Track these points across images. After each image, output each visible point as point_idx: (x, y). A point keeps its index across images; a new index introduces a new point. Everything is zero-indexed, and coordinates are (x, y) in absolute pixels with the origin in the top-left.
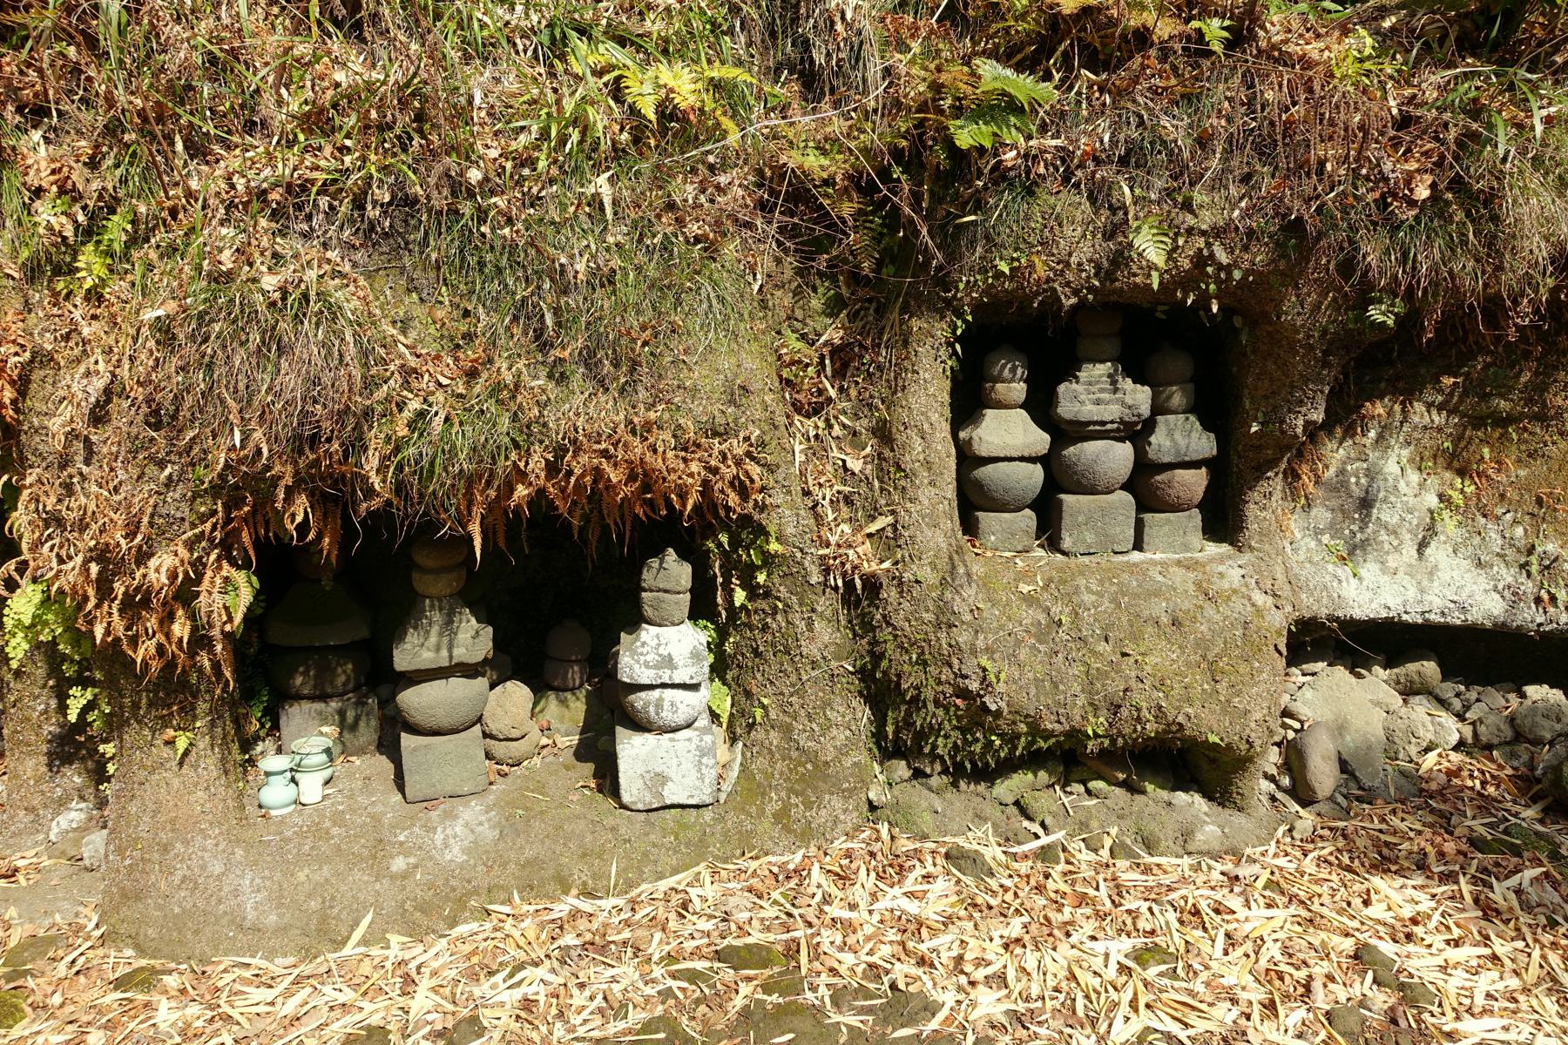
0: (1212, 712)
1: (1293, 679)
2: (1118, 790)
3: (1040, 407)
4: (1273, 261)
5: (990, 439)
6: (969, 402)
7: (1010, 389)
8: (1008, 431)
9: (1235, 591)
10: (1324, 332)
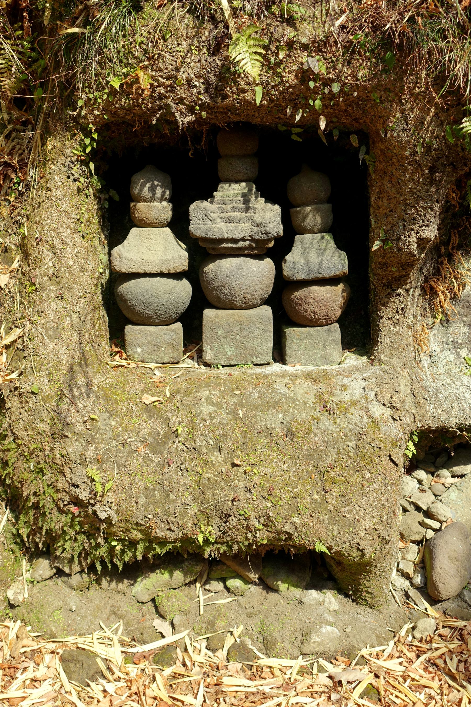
0: (320, 521)
1: (442, 480)
2: (254, 588)
3: (179, 225)
4: (375, 75)
5: (128, 255)
6: (117, 222)
7: (150, 209)
8: (152, 248)
9: (354, 403)
10: (428, 148)
